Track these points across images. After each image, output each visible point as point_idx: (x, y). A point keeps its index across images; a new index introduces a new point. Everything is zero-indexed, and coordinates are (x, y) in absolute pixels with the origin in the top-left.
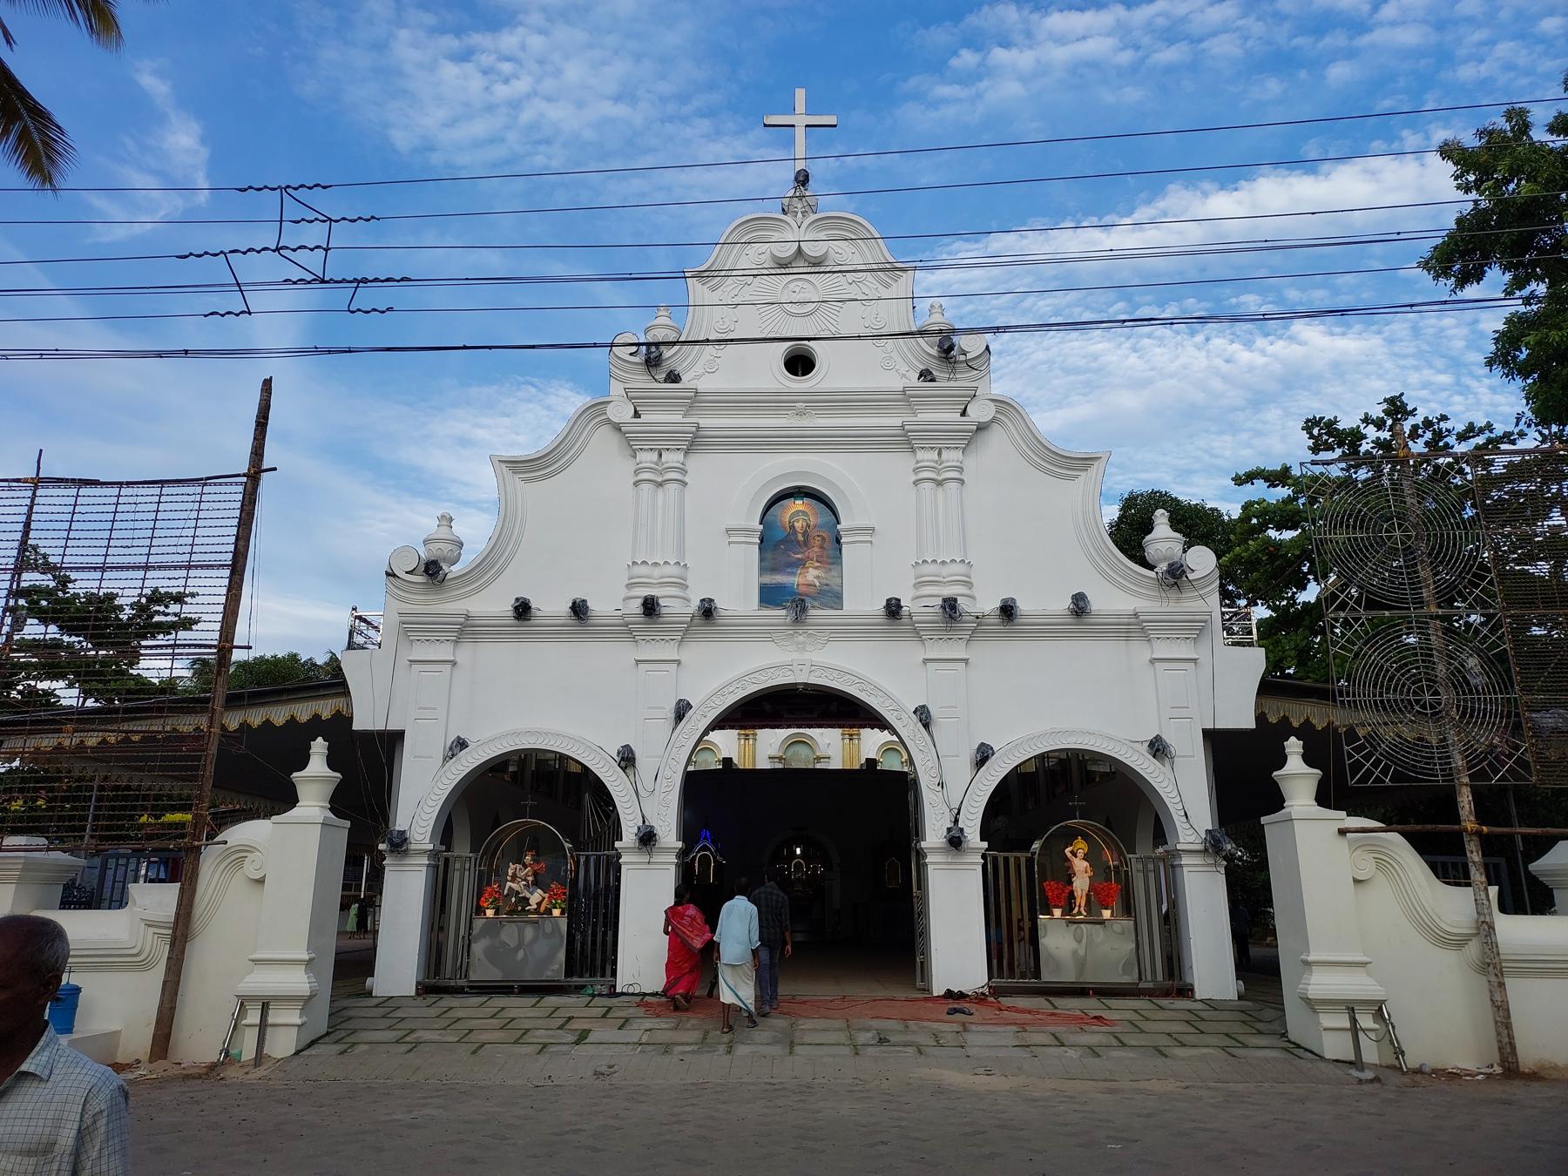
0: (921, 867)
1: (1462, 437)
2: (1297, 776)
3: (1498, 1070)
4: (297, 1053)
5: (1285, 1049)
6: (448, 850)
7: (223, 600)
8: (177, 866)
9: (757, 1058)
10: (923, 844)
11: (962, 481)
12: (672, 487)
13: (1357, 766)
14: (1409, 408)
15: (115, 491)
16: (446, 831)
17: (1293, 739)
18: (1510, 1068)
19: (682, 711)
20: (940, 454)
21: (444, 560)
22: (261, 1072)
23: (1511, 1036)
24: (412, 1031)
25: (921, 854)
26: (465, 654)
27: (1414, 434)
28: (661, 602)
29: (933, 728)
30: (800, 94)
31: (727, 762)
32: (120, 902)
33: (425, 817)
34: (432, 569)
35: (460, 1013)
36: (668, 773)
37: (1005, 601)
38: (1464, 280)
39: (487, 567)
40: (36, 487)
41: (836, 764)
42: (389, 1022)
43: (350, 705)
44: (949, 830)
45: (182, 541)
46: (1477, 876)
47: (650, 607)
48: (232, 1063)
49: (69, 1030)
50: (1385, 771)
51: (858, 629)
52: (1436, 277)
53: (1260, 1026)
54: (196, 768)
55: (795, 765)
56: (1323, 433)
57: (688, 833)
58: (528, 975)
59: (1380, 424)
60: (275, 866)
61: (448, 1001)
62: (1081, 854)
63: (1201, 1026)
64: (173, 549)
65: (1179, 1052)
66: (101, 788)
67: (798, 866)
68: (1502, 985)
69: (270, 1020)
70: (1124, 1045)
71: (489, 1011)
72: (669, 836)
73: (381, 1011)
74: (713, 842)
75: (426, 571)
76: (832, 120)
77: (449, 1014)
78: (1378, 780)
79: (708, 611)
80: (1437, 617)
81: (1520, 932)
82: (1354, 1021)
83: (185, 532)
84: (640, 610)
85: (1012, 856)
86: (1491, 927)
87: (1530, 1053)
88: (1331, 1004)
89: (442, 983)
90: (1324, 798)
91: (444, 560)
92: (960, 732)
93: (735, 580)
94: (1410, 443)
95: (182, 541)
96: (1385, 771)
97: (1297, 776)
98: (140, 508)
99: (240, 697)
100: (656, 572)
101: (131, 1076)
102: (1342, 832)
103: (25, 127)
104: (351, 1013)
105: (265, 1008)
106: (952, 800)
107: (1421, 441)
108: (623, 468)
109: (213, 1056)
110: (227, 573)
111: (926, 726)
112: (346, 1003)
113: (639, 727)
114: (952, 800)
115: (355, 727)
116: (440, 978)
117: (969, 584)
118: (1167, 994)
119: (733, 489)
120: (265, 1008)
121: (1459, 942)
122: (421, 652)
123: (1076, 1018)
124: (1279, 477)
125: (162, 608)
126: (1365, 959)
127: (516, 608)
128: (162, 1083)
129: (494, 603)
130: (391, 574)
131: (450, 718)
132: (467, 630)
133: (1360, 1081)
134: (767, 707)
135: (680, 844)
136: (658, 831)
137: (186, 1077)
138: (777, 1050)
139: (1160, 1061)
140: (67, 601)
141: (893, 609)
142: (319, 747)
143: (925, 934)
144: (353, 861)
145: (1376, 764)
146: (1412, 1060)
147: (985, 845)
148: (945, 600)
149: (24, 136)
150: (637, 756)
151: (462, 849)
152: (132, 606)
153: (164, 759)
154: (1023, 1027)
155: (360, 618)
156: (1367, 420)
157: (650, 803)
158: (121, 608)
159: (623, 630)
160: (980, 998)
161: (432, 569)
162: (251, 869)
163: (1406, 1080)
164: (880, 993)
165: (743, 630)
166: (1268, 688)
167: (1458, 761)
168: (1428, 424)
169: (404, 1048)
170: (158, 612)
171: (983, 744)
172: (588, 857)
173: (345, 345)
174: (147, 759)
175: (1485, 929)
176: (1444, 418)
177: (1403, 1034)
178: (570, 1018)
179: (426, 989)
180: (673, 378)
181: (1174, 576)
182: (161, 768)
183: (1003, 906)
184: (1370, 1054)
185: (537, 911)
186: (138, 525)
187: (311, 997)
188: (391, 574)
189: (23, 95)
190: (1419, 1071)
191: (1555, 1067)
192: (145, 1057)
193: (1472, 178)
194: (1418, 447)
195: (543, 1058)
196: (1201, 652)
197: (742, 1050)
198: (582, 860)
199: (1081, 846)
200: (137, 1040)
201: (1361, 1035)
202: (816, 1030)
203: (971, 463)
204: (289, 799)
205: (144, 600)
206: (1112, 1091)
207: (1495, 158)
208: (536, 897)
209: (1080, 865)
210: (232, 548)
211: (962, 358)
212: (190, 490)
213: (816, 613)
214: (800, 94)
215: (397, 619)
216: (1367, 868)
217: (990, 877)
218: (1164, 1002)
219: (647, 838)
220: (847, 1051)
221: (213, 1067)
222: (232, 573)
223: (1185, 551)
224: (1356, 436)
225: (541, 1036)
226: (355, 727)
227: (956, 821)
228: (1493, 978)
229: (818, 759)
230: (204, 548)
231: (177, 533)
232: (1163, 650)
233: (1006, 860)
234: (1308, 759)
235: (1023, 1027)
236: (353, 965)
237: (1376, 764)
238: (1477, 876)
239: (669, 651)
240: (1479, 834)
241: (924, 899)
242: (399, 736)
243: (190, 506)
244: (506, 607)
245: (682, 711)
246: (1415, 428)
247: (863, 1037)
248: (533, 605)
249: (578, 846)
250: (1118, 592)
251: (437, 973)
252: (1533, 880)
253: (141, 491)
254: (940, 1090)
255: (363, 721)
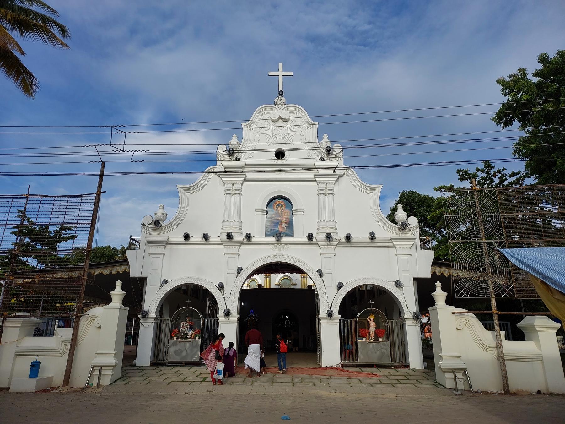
0: (319, 324)
1: (512, 175)
2: (440, 295)
3: (503, 392)
4: (111, 384)
5: (434, 385)
6: (161, 317)
7: (88, 235)
8: (68, 322)
9: (260, 386)
10: (319, 316)
11: (334, 194)
12: (237, 196)
13: (458, 292)
14: (492, 166)
15: (53, 199)
16: (161, 311)
17: (438, 282)
18: (507, 391)
19: (240, 270)
20: (326, 185)
21: (161, 220)
22: (99, 390)
23: (507, 381)
24: (149, 377)
25: (319, 319)
26: (167, 251)
27: (495, 175)
28: (233, 234)
29: (323, 277)
30: (281, 65)
31: (260, 286)
32: (52, 334)
33: (153, 306)
34: (157, 223)
35: (165, 372)
36: (235, 291)
37: (347, 234)
38: (506, 124)
39: (175, 222)
40: (28, 198)
41: (299, 287)
42: (140, 374)
43: (129, 268)
44: (328, 311)
45: (75, 215)
46: (497, 328)
47: (229, 236)
48: (89, 387)
49: (37, 376)
50: (467, 293)
51: (299, 243)
52: (497, 124)
53: (428, 378)
54: (79, 290)
55: (284, 287)
56: (464, 175)
57: (242, 310)
58: (189, 359)
59: (483, 171)
60: (104, 322)
61: (161, 368)
62: (372, 319)
63: (409, 377)
64: (72, 218)
65: (399, 385)
66: (45, 297)
67: (287, 322)
68: (504, 364)
69: (102, 373)
70: (382, 383)
71: (173, 371)
72: (235, 313)
73: (138, 371)
74: (254, 314)
75: (155, 224)
76: (291, 74)
77: (161, 372)
78: (465, 296)
79: (248, 237)
80: (485, 242)
81: (512, 347)
82: (455, 375)
83: (76, 213)
84: (226, 237)
85: (349, 320)
86: (501, 345)
87: (514, 386)
88: (448, 369)
89: (159, 361)
90: (448, 302)
91: (161, 220)
92: (332, 277)
93: (257, 226)
94: (493, 178)
95: (75, 215)
96: (467, 293)
97: (440, 295)
98: (61, 204)
99: (93, 265)
100: (232, 224)
101: (57, 391)
102: (453, 313)
103: (24, 77)
104: (129, 371)
105: (101, 369)
106: (329, 300)
107: (497, 177)
108: (221, 188)
109: (83, 385)
110: (90, 226)
111: (321, 276)
112: (127, 368)
113: (226, 275)
114: (329, 300)
115: (131, 275)
116: (158, 361)
117: (336, 229)
118: (400, 367)
119: (258, 194)
120: (101, 369)
121: (491, 350)
122: (153, 251)
123: (368, 374)
124: (450, 189)
125: (64, 232)
126: (460, 355)
127: (185, 236)
128: (66, 393)
129: (177, 235)
130: (143, 225)
131: (164, 271)
132: (168, 243)
133: (456, 395)
134: (274, 267)
135: (238, 316)
136: (231, 311)
137: (75, 392)
138: (268, 384)
139: (392, 388)
140: (32, 229)
141: (310, 237)
142: (119, 283)
143: (320, 346)
144: (130, 320)
145: (465, 291)
146: (475, 388)
147: (340, 316)
148: (327, 234)
149: (23, 80)
150: (225, 286)
151: (166, 317)
152: (54, 231)
153: (68, 287)
154: (350, 377)
155: (133, 239)
156: (478, 170)
157: (229, 302)
158: (50, 232)
159: (221, 243)
160: (337, 368)
161: (157, 223)
162: (96, 323)
163: (471, 395)
164: (305, 366)
165: (260, 243)
166: (436, 263)
167: (491, 290)
168: (499, 171)
169: (146, 383)
170: (63, 234)
171: (340, 282)
172: (211, 320)
173: (131, 172)
174: (63, 287)
175: (499, 345)
176: (504, 169)
177: (472, 380)
178: (201, 374)
179: (153, 364)
180: (238, 159)
181: (403, 227)
182: (68, 291)
183: (350, 336)
184: (461, 386)
185: (190, 338)
186: (61, 210)
187: (115, 366)
188: (143, 225)
189: (23, 67)
190: (477, 392)
191: (522, 391)
192: (61, 385)
193: (507, 91)
194: (496, 180)
195: (191, 386)
196: (412, 251)
197: (256, 384)
198: (206, 320)
199: (372, 317)
200: (59, 380)
201: (457, 380)
202: (281, 378)
203: (336, 188)
204: (108, 300)
205: (58, 229)
206: (374, 398)
207: (515, 85)
208: (190, 333)
209: (372, 323)
210: (91, 218)
211: (334, 153)
212: (78, 199)
213: (284, 239)
214: (281, 65)
215: (145, 240)
216: (461, 325)
217: (342, 327)
218: (399, 370)
219: (227, 314)
220: (290, 384)
221: (83, 388)
222: (91, 226)
223: (408, 217)
224: (475, 176)
225: (191, 379)
226: (131, 275)
227: (331, 308)
228: (501, 362)
229: (293, 285)
230: (82, 218)
231: (73, 213)
232: (400, 251)
233: (347, 321)
234: (443, 289)
235: (350, 377)
236: (129, 358)
237: (465, 291)
238: (497, 328)
239: (235, 251)
240: (498, 314)
241: (320, 334)
242: (146, 278)
243: (78, 204)
244: (181, 236)
245: (240, 270)
246: (495, 172)
247: (296, 380)
248: (190, 235)
249: (205, 316)
250: (384, 231)
251: (157, 358)
252: (518, 329)
253: (62, 199)
254: (318, 397)
255: (133, 274)
